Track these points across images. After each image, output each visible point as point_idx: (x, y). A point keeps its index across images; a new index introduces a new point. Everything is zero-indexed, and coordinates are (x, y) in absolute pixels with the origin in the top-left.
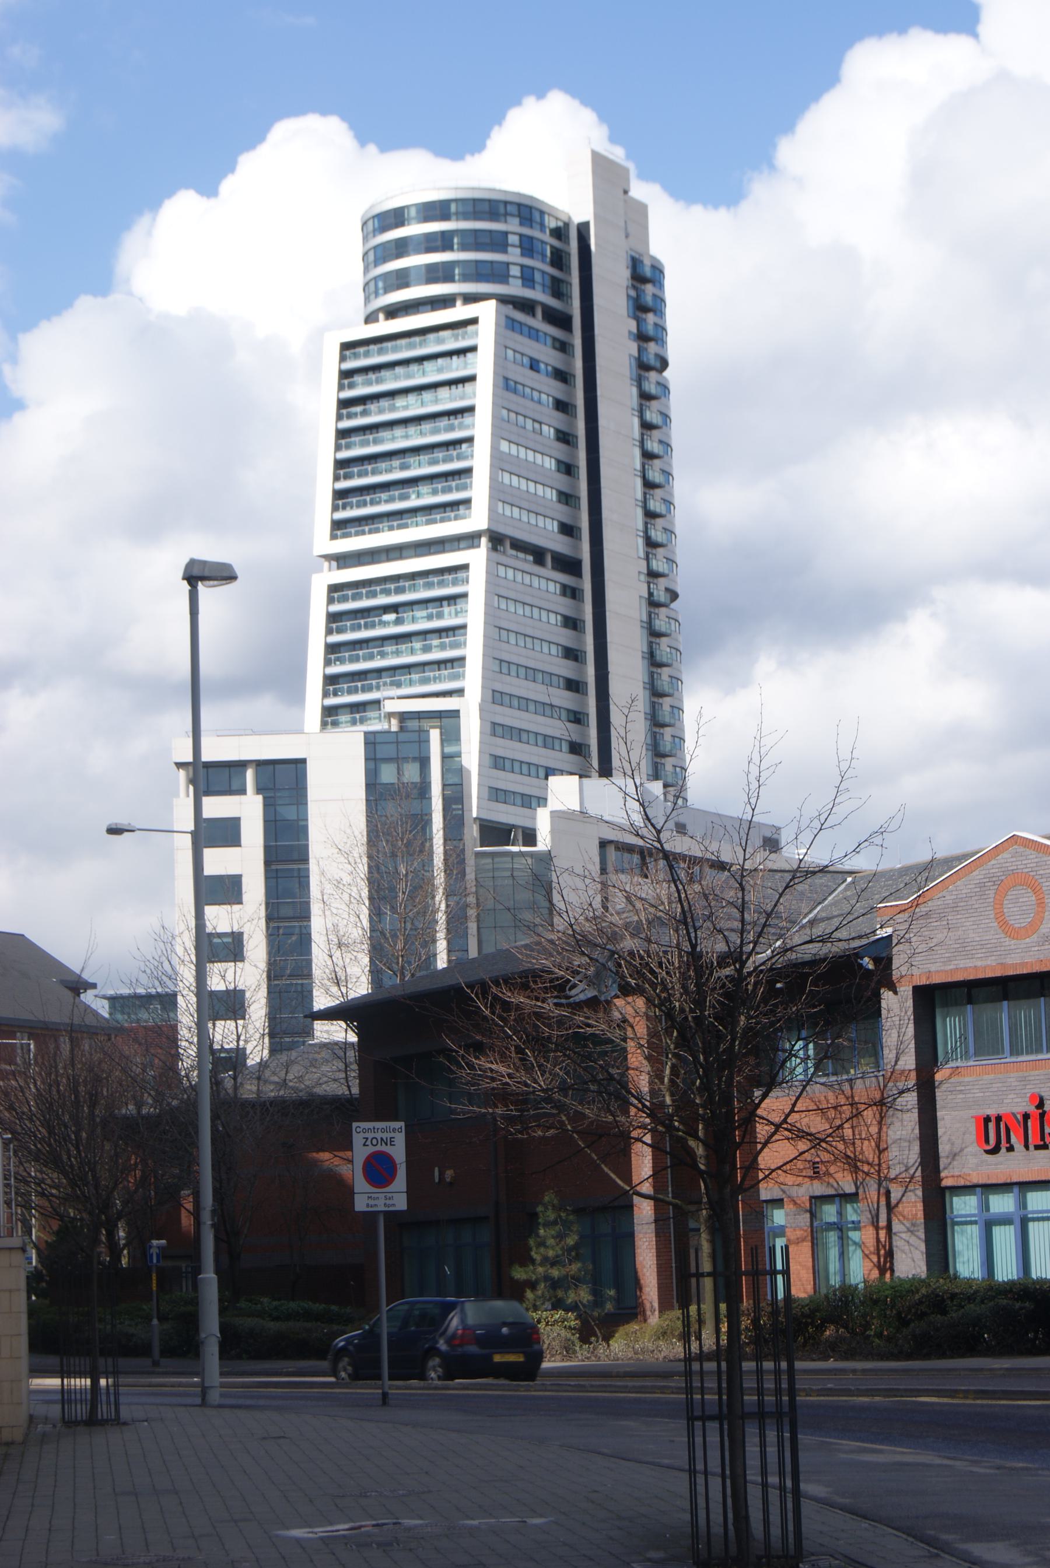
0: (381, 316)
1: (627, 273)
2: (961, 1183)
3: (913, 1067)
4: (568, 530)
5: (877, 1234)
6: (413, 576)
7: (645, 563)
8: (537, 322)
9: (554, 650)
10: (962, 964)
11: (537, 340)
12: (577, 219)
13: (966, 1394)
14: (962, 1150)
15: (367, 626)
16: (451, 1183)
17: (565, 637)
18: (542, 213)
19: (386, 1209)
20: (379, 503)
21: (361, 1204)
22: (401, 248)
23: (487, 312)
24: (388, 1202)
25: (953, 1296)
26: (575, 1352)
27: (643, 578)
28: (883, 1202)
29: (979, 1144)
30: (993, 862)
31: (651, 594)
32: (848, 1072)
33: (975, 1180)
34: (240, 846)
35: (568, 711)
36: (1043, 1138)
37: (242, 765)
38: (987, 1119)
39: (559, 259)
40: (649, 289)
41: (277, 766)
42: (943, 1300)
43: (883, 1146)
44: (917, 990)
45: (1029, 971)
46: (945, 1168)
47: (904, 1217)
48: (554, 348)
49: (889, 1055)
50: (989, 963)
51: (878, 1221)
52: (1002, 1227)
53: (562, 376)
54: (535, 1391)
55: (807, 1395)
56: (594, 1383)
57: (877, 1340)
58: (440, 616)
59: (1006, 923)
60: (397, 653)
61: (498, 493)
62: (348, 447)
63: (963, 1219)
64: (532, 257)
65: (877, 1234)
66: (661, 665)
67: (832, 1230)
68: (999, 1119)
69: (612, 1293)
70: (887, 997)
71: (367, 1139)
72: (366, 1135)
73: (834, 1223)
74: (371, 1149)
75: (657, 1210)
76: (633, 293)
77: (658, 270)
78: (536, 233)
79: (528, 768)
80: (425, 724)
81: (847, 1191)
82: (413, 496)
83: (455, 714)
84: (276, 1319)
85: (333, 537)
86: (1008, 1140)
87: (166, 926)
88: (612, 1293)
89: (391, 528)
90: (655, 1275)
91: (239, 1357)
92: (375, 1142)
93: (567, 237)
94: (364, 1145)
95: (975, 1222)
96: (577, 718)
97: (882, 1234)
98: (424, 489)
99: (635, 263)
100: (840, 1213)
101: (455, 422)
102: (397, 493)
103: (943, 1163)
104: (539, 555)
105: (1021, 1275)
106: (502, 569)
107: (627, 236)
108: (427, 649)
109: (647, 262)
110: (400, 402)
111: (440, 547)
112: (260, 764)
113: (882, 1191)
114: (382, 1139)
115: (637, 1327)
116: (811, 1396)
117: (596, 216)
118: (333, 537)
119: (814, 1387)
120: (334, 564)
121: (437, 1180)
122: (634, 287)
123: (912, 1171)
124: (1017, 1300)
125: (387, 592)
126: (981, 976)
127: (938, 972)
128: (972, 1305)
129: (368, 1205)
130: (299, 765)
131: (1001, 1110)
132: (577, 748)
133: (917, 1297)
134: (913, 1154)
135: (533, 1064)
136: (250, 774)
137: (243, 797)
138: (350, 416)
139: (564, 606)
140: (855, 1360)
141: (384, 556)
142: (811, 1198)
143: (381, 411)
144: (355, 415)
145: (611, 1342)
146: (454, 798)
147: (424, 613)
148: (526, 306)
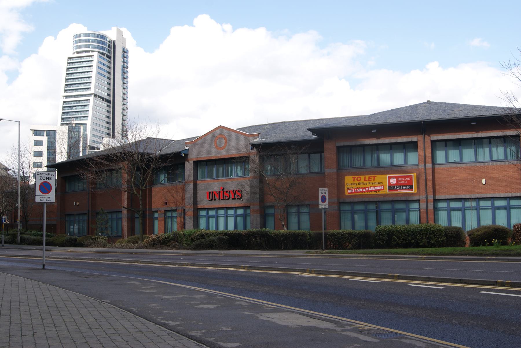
0: (76, 53)
1: (122, 50)
2: (203, 207)
3: (192, 180)
4: (109, 95)
5: (181, 219)
6: (79, 101)
7: (122, 102)
8: (105, 57)
9: (105, 116)
10: (206, 156)
11: (105, 60)
12: (113, 40)
13: (244, 268)
14: (203, 200)
15: (70, 109)
16: (78, 206)
17: (107, 114)
18: (107, 38)
19: (47, 201)
20: (74, 87)
21: (38, 199)
22: (80, 41)
23: (96, 54)
24: (48, 199)
25: (207, 234)
26: (106, 246)
27: (122, 105)
28: (183, 212)
29: (207, 198)
30: (214, 132)
31: (123, 108)
32: (175, 181)
33: (206, 207)
34: (42, 146)
35: (107, 127)
36: (223, 197)
37: (44, 131)
38: (210, 193)
39: (109, 46)
40: (126, 54)
41: (51, 132)
42: (204, 235)
43: (183, 199)
44: (194, 162)
45: (222, 158)
46: (199, 204)
47: (188, 215)
48: (108, 62)
49: (186, 177)
50: (212, 156)
51: (181, 216)
52: (212, 218)
53: (109, 78)
54: (97, 261)
55: (186, 266)
56: (115, 259)
57: (185, 245)
58: (84, 108)
59: (217, 146)
60: (76, 115)
61: (96, 87)
62: (68, 76)
63: (202, 216)
64: (105, 45)
65: (181, 219)
66: (124, 121)
67: (169, 218)
68: (213, 193)
69: (322, 206)
70: (187, 164)
71: (41, 177)
72: (41, 176)
73: (170, 217)
74: (42, 181)
75: (128, 212)
76: (123, 54)
77: (127, 50)
78: (106, 41)
79: (98, 137)
80: (80, 126)
81: (174, 209)
82: (80, 86)
83: (86, 124)
84: (35, 236)
85: (64, 93)
86: (215, 198)
87: (14, 146)
88: (322, 206)
89: (76, 92)
90: (126, 228)
91: (24, 244)
92: (44, 178)
93: (111, 43)
94: (40, 179)
95: (205, 217)
96: (108, 129)
97: (182, 219)
98: (82, 85)
99: (123, 49)
100: (172, 214)
101: (88, 84)
102: (77, 85)
103: (198, 202)
104: (103, 99)
105: (478, 226)
106: (96, 101)
107: (122, 44)
108: (81, 114)
109: (125, 49)
110: (78, 69)
111: (85, 96)
112: (47, 131)
113: (183, 209)
114: (47, 177)
115: (122, 240)
116: (187, 266)
117: (117, 39)
118: (64, 93)
119: (189, 263)
120: (64, 98)
121: (75, 205)
122: (123, 58)
123: (191, 205)
124: (224, 236)
125: (74, 103)
126: (210, 159)
127: (199, 158)
128: (212, 237)
129: (40, 200)
130: (55, 132)
131: (213, 191)
132: (108, 134)
133: (197, 234)
134: (192, 200)
135: (99, 175)
136: (45, 132)
137: (43, 137)
138: (69, 71)
139: (107, 108)
140: (180, 250)
141: (74, 97)
142: (165, 210)
143: (75, 70)
144: (70, 71)
145: (116, 243)
146: (85, 143)
147: (81, 108)
148: (103, 54)
